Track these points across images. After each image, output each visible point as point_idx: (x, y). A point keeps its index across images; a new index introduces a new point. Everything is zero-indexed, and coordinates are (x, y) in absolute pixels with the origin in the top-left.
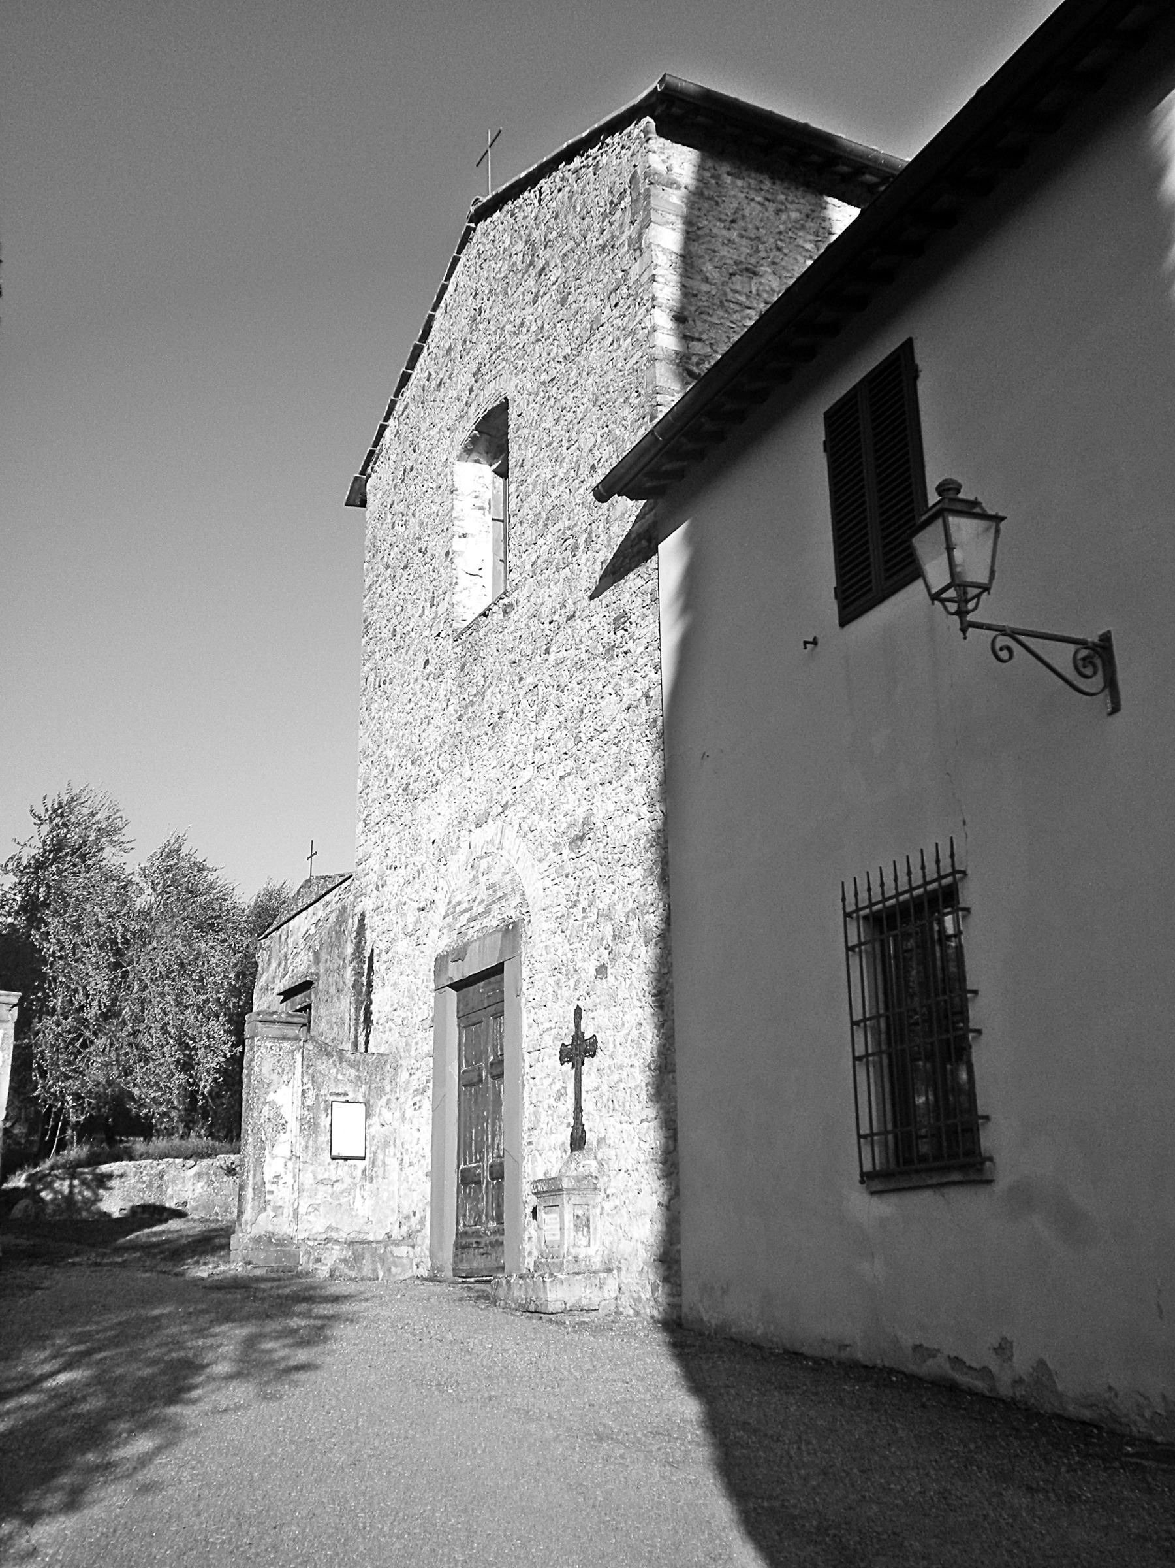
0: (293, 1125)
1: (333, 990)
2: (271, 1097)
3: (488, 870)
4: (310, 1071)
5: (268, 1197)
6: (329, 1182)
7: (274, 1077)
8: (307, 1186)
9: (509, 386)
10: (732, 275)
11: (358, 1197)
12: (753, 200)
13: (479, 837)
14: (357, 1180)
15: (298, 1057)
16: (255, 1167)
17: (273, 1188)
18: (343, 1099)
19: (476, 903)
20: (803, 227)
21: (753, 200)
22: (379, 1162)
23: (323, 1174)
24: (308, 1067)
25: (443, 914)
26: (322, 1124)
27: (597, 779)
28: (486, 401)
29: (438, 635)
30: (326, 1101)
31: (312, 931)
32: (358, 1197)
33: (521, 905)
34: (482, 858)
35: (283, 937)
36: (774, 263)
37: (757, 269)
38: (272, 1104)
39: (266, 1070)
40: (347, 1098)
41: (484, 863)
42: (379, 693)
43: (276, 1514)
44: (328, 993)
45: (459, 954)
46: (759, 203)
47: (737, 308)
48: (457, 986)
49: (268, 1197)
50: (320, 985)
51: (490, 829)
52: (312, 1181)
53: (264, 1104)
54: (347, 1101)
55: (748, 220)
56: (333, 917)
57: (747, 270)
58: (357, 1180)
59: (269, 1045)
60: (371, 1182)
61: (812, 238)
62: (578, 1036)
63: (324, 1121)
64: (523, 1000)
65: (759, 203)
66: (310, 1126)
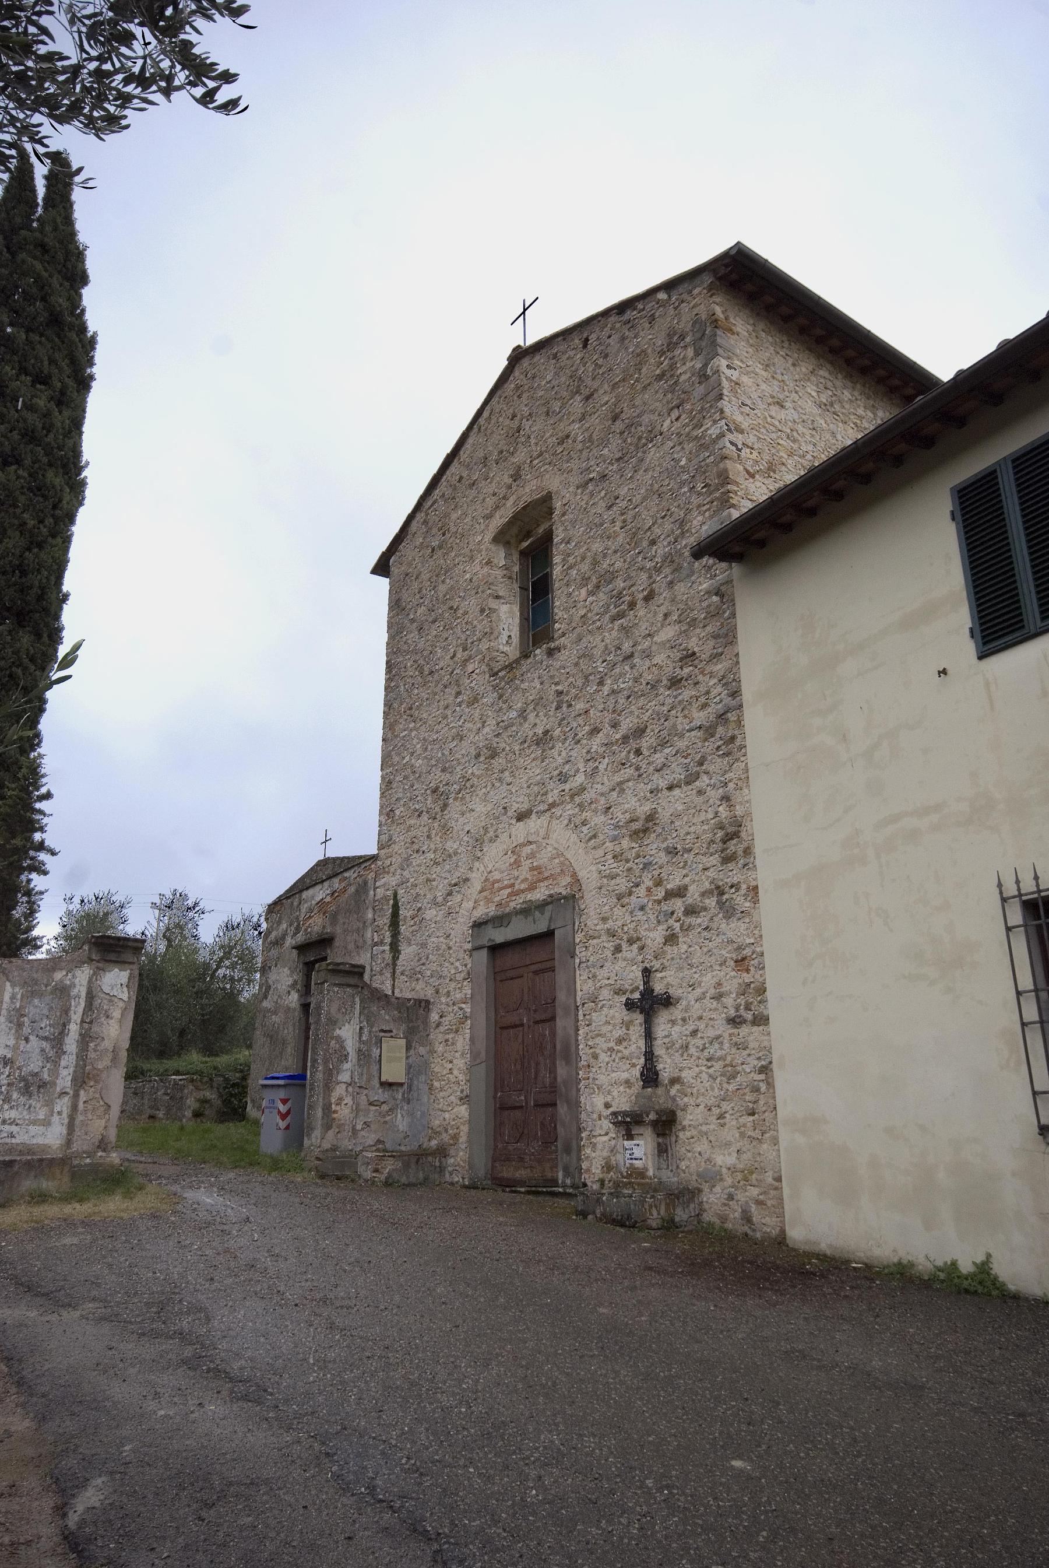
0: (352, 1055)
1: (351, 946)
2: (338, 1032)
3: (532, 856)
4: (366, 1012)
5: (335, 1116)
6: (378, 1103)
7: (340, 1016)
8: (362, 1107)
9: (553, 482)
10: (769, 404)
11: (399, 1116)
12: (778, 353)
13: (520, 831)
14: (398, 1102)
15: (357, 1000)
16: (324, 1091)
17: (338, 1108)
18: (389, 1035)
19: (518, 882)
20: (809, 380)
21: (778, 353)
22: (414, 1088)
23: (374, 1097)
24: (364, 1008)
25: (479, 888)
26: (374, 1055)
27: (663, 784)
28: (528, 491)
29: (473, 672)
30: (376, 1037)
31: (328, 899)
32: (399, 1116)
33: (571, 884)
34: (525, 845)
35: (295, 904)
36: (794, 402)
37: (784, 404)
38: (338, 1039)
39: (333, 1010)
40: (392, 1034)
41: (528, 849)
42: (405, 717)
43: (616, 1467)
44: (346, 948)
45: (500, 920)
46: (782, 356)
47: (774, 429)
48: (495, 949)
49: (335, 1116)
50: (337, 943)
51: (534, 824)
52: (366, 1103)
53: (332, 1038)
54: (392, 1037)
55: (777, 366)
56: (352, 889)
57: (778, 403)
58: (398, 1102)
59: (336, 989)
60: (408, 1103)
61: (815, 388)
62: (648, 992)
63: (375, 1052)
64: (577, 961)
65: (782, 356)
66: (363, 1056)
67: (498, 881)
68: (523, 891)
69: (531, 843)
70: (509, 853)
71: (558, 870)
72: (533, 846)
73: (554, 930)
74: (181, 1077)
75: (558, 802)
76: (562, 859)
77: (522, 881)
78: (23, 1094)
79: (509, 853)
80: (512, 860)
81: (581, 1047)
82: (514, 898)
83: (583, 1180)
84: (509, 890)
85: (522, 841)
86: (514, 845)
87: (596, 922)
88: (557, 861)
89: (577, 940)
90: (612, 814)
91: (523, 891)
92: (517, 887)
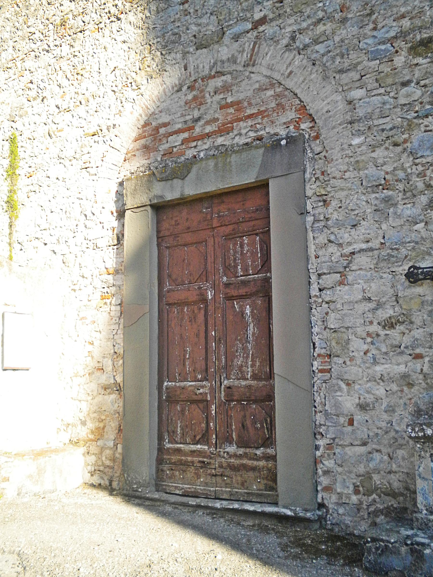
41: (218, 82)
67: (165, 125)
68: (208, 135)
69: (220, 74)
70: (185, 88)
71: (273, 105)
72: (228, 78)
73: (268, 180)
74: (189, 486)
75: (271, 16)
76: (278, 90)
77: (208, 123)
78: (279, 43)
79: (185, 88)
80: (190, 97)
81: (315, 330)
82: (194, 144)
83: (319, 500)
84: (186, 135)
85: (207, 72)
86: (193, 79)
87: (343, 168)
88: (270, 93)
89: (309, 193)
90: (375, 22)
91: (208, 135)
92: (198, 130)
